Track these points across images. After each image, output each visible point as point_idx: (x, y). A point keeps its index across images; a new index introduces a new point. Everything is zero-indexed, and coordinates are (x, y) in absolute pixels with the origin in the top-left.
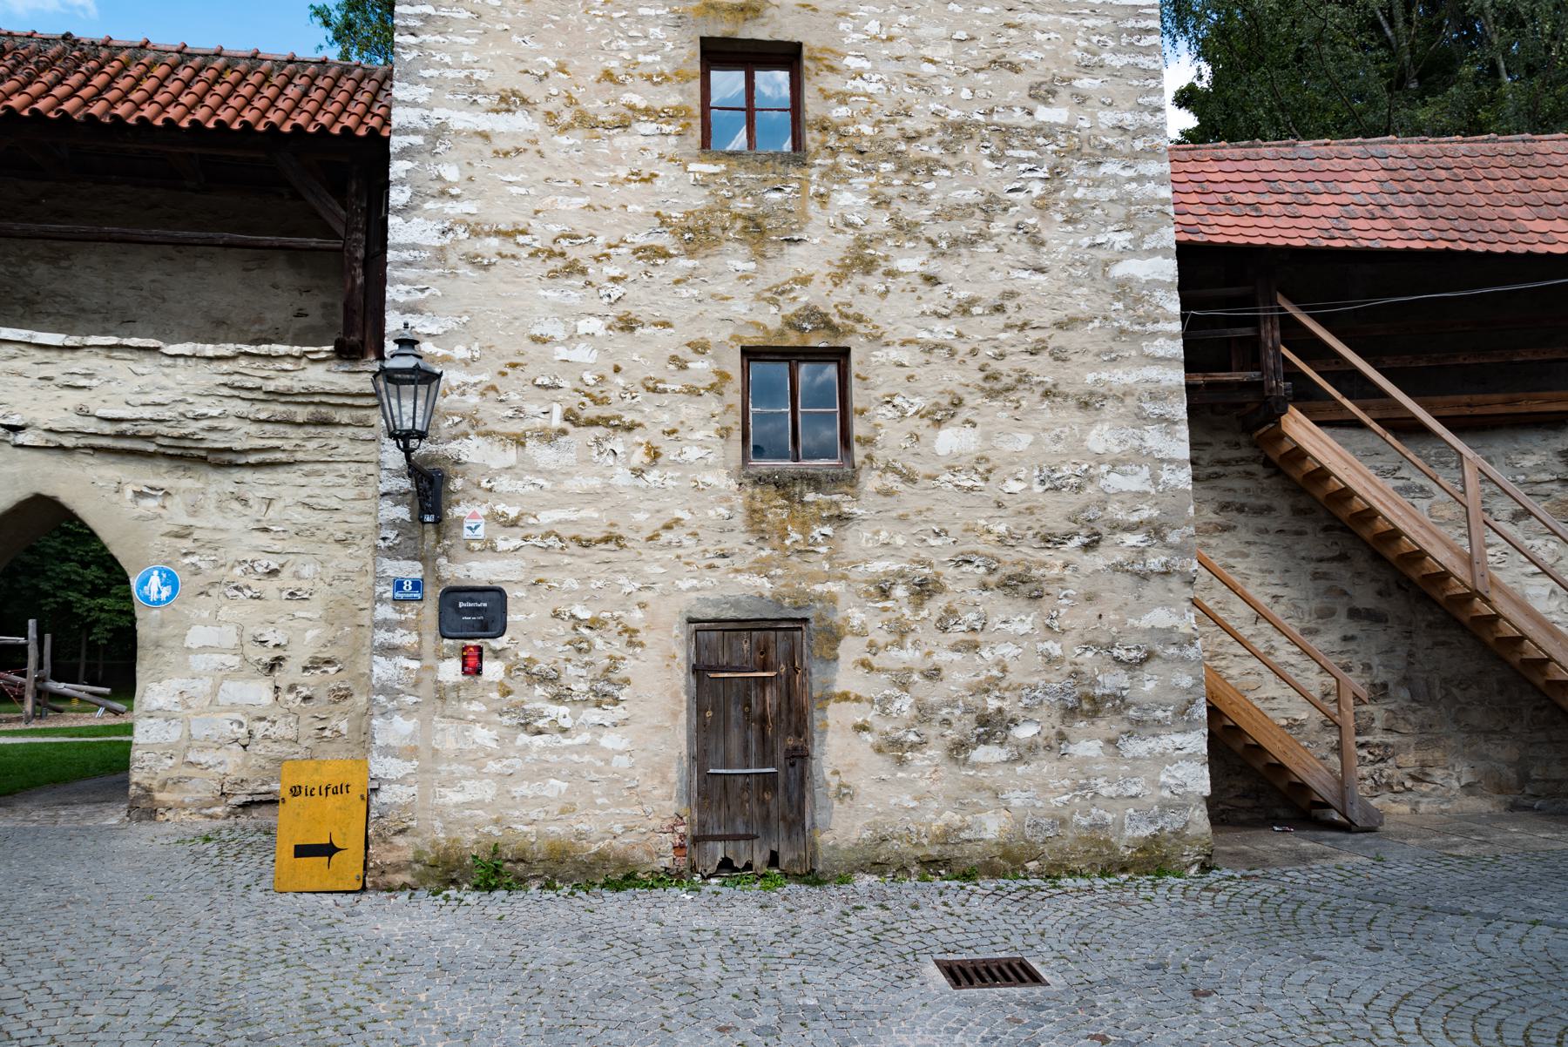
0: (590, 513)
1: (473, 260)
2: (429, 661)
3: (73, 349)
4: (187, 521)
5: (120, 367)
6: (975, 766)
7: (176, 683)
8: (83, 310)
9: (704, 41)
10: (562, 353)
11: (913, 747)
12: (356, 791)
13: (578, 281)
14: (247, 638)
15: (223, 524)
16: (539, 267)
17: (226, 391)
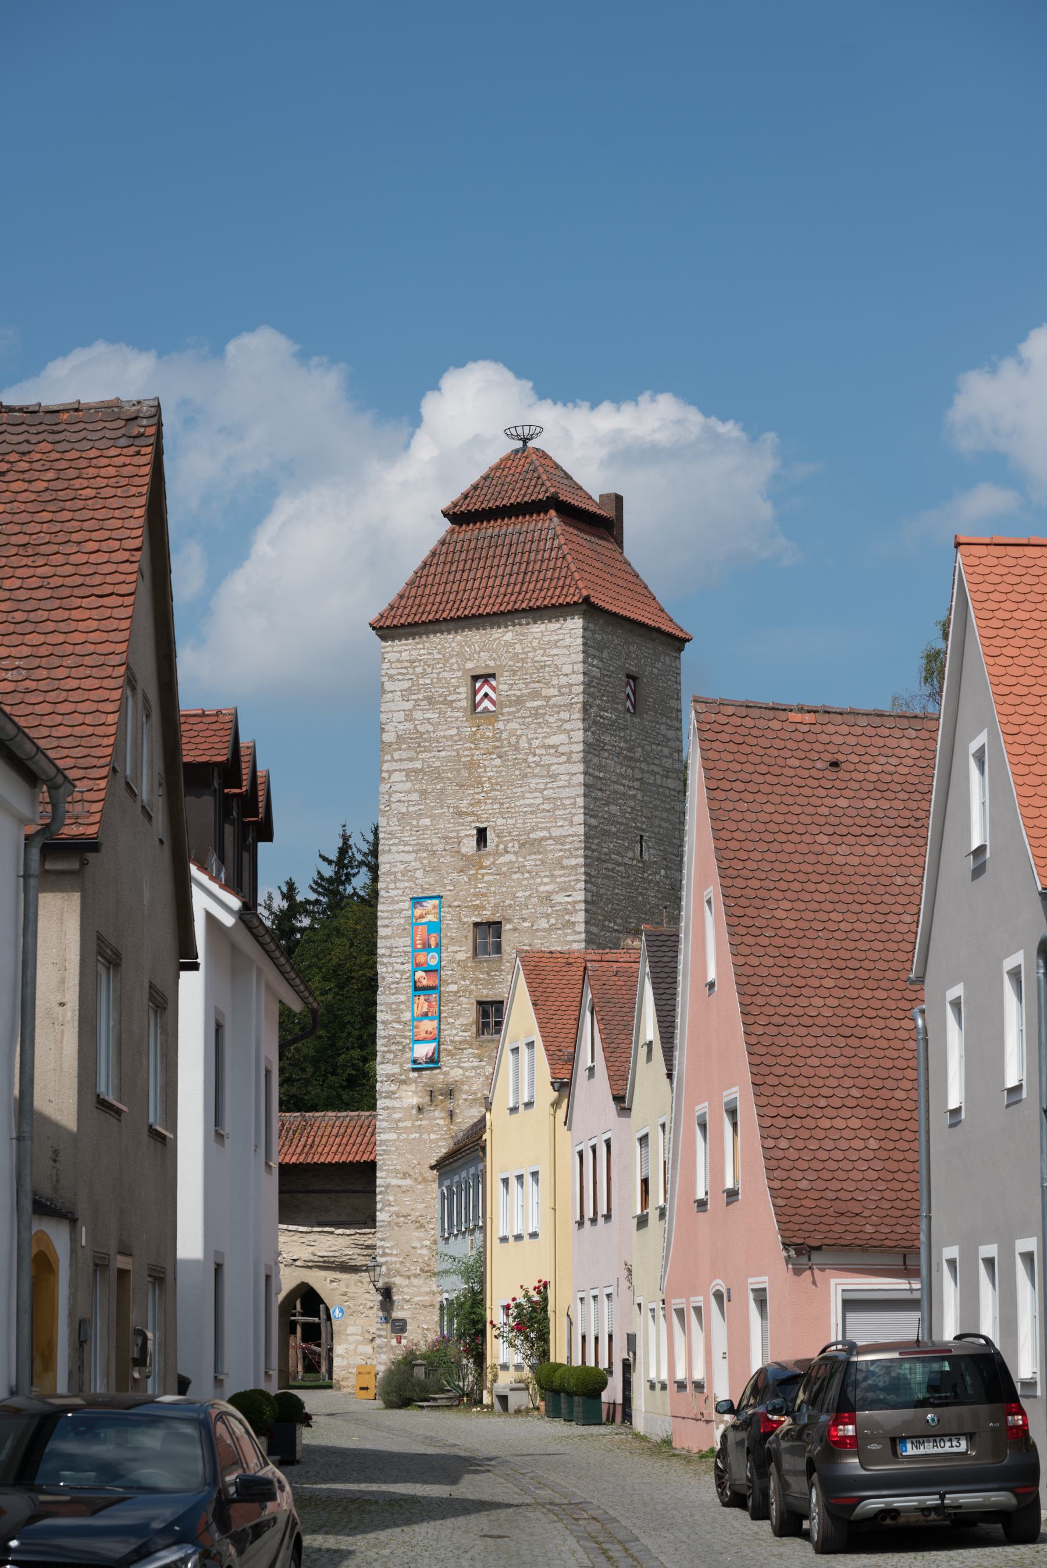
1: (397, 1224)
3: (309, 1233)
5: (323, 1238)
7: (345, 1346)
10: (419, 1251)
13: (423, 1230)
15: (356, 1291)
16: (413, 1226)
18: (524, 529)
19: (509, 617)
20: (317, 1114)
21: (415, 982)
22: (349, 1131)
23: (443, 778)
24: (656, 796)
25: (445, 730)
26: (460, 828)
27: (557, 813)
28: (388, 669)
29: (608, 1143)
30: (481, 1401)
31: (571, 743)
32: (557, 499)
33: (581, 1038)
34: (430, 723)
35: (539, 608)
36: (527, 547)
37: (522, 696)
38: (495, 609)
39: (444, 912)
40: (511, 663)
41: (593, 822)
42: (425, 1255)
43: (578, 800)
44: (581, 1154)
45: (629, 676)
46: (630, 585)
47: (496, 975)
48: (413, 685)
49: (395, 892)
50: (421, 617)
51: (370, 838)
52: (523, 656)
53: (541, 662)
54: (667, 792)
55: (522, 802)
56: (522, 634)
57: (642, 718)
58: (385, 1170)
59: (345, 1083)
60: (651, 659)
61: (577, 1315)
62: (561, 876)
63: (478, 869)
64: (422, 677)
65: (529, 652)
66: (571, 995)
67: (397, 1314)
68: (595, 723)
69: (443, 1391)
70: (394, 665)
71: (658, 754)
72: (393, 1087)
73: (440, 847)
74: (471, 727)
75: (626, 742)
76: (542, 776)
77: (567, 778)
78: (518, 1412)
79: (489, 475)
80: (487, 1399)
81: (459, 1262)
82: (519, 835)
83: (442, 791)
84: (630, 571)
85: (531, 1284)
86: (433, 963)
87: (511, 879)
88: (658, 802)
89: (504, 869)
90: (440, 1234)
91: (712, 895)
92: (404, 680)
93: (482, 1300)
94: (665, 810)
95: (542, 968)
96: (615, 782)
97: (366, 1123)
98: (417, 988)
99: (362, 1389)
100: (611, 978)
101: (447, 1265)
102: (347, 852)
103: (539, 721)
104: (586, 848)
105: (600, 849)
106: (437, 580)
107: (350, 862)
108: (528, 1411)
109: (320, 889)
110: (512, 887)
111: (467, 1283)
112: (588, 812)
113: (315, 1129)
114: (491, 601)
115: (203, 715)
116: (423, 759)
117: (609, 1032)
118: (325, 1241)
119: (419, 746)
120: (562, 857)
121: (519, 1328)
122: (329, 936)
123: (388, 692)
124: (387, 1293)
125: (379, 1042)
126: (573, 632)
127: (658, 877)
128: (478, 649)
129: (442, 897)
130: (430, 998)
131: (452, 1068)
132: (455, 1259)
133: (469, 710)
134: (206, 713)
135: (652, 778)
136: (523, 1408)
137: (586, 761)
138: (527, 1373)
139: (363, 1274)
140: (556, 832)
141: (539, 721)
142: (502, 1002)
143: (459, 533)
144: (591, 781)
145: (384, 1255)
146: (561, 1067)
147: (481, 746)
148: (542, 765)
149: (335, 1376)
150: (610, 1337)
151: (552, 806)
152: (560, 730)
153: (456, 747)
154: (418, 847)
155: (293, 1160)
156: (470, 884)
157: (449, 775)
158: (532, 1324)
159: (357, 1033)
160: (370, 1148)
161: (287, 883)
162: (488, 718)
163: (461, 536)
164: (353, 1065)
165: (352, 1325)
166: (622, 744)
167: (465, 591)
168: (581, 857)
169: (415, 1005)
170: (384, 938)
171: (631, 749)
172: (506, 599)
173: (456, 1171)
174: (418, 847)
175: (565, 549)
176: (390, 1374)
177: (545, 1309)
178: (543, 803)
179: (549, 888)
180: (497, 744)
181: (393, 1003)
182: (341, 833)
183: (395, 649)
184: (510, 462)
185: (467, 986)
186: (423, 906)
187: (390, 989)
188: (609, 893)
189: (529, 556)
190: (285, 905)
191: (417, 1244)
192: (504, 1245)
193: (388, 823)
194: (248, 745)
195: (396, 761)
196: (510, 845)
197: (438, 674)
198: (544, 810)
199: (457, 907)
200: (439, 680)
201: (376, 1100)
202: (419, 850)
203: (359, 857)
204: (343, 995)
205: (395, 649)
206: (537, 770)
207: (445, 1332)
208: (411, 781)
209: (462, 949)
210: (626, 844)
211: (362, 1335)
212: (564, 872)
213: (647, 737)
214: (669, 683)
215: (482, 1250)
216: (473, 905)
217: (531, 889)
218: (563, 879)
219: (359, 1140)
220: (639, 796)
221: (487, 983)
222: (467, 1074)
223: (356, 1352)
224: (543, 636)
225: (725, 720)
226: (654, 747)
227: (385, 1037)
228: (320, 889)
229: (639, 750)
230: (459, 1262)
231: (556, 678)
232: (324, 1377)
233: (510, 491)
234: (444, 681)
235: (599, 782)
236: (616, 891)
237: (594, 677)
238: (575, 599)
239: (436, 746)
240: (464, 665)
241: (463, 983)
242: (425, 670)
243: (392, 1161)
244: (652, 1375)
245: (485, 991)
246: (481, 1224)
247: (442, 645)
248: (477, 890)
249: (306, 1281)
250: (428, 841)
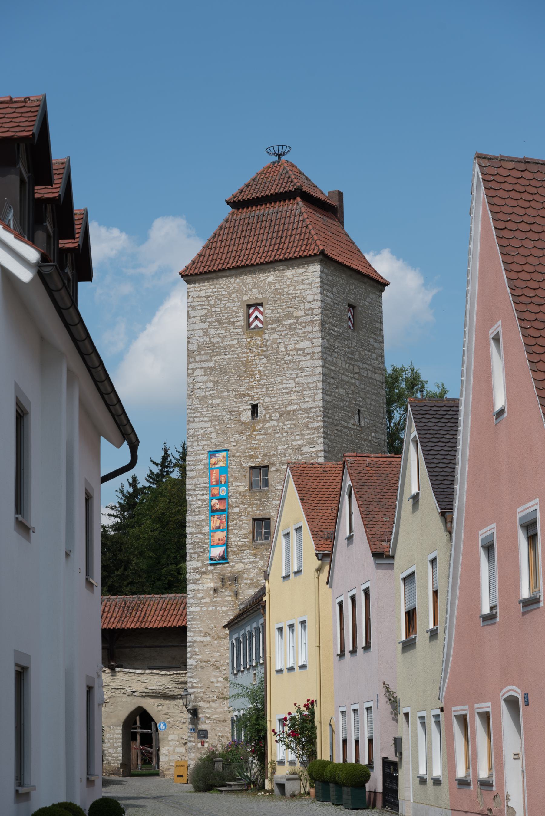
0: (221, 716)
1: (201, 667)
3: (143, 674)
4: (167, 711)
5: (152, 677)
7: (167, 748)
9: (454, 405)
10: (216, 685)
12: (186, 766)
13: (218, 670)
15: (174, 712)
16: (212, 668)
18: (280, 210)
19: (271, 265)
20: (148, 596)
21: (212, 507)
22: (169, 607)
23: (228, 372)
24: (368, 385)
25: (230, 341)
26: (240, 405)
27: (305, 393)
28: (191, 302)
29: (367, 592)
30: (263, 787)
31: (313, 347)
32: (302, 190)
33: (340, 517)
34: (219, 337)
35: (291, 258)
36: (282, 222)
37: (280, 317)
38: (262, 261)
39: (230, 460)
40: (273, 296)
41: (329, 399)
42: (220, 687)
43: (318, 384)
44: (341, 605)
45: (350, 306)
46: (349, 248)
47: (265, 501)
48: (208, 312)
49: (198, 448)
50: (213, 268)
51: (181, 450)
52: (281, 291)
53: (292, 294)
54: (375, 382)
55: (281, 386)
56: (280, 277)
57: (358, 333)
58: (193, 631)
59: (166, 586)
60: (364, 295)
61: (338, 724)
62: (308, 434)
63: (253, 431)
64: (214, 307)
65: (285, 288)
66: (328, 493)
67: (202, 727)
68: (329, 334)
69: (235, 779)
70: (195, 300)
71: (369, 357)
72: (198, 577)
73: (227, 418)
74: (247, 338)
75: (349, 348)
76: (294, 369)
77: (311, 369)
78: (293, 796)
79: (256, 177)
80: (268, 786)
81: (247, 689)
82: (280, 408)
83: (228, 381)
84: (349, 240)
85: (302, 702)
86: (223, 493)
87: (275, 438)
88: (370, 389)
89: (270, 431)
90: (231, 671)
91: (500, 330)
92: (202, 309)
93: (264, 715)
94: (374, 394)
95: (306, 475)
96: (342, 374)
97: (180, 601)
98: (213, 511)
99: (178, 776)
100: (365, 469)
101: (236, 691)
102: (167, 459)
104: (324, 416)
105: (333, 417)
106: (223, 244)
107: (169, 464)
108: (301, 795)
109: (151, 480)
110: (275, 442)
111: (252, 703)
112: (325, 392)
113: (146, 606)
114: (259, 256)
115: (11, 101)
116: (215, 361)
117: (366, 506)
118: (153, 679)
119: (213, 352)
120: (308, 422)
121: (293, 734)
122: (156, 497)
123: (192, 317)
124: (194, 712)
125: (188, 547)
126: (313, 274)
127: (370, 438)
128: (251, 287)
129: (228, 450)
130: (222, 517)
131: (237, 563)
132: (244, 687)
133: (245, 327)
134: (14, 100)
135: (366, 372)
136: (296, 793)
137: (323, 359)
138: (298, 767)
139: (179, 700)
140: (304, 406)
142: (269, 519)
143: (237, 214)
144: (327, 372)
145: (193, 687)
146: (323, 543)
147: (254, 350)
148: (294, 362)
149: (161, 768)
150: (370, 741)
151: (301, 388)
152: (306, 339)
153: (236, 352)
154: (213, 418)
155: (132, 626)
156: (248, 441)
157: (233, 370)
158: (303, 732)
159: (173, 555)
160: (182, 618)
161: (132, 477)
162: (258, 332)
163: (239, 216)
164: (172, 575)
166: (347, 349)
167: (242, 250)
168: (321, 421)
169: (212, 522)
170: (191, 478)
171: (352, 353)
172: (269, 254)
173: (242, 627)
174: (213, 418)
175: (308, 221)
176: (198, 768)
177: (312, 721)
178: (295, 387)
179: (300, 442)
180: (264, 349)
181: (197, 521)
182: (163, 447)
183: (196, 289)
184: (270, 169)
185: (246, 509)
186: (216, 457)
187: (195, 511)
188: (339, 446)
189: (283, 227)
190: (131, 490)
191: (214, 680)
192: (280, 675)
193: (193, 403)
194: (63, 161)
195: (197, 362)
196: (273, 415)
197: (225, 304)
198: (296, 391)
199: (238, 457)
200: (226, 308)
201: (186, 585)
202: (213, 420)
203: (174, 461)
204: (164, 532)
205: (196, 289)
206: (291, 365)
207: (235, 738)
208: (208, 375)
209: (242, 484)
210: (350, 415)
211: (178, 740)
212: (310, 432)
213: (362, 346)
214: (375, 312)
215: (263, 679)
217: (288, 444)
218: (309, 436)
219: (175, 612)
220: (358, 383)
221: (259, 506)
222: (246, 567)
224: (294, 277)
225: (507, 173)
226: (366, 352)
227: (192, 544)
228: (151, 480)
229: (357, 353)
230: (247, 689)
231: (303, 304)
232: (155, 767)
233: (270, 187)
234: (228, 309)
235: (332, 373)
236: (344, 445)
237: (328, 304)
238: (315, 252)
239: (224, 352)
240: (242, 298)
241: (243, 506)
242: (216, 302)
243: (197, 625)
244: (422, 771)
245: (258, 512)
246: (262, 661)
247: (227, 286)
248: (252, 445)
249: (141, 706)
250: (219, 414)
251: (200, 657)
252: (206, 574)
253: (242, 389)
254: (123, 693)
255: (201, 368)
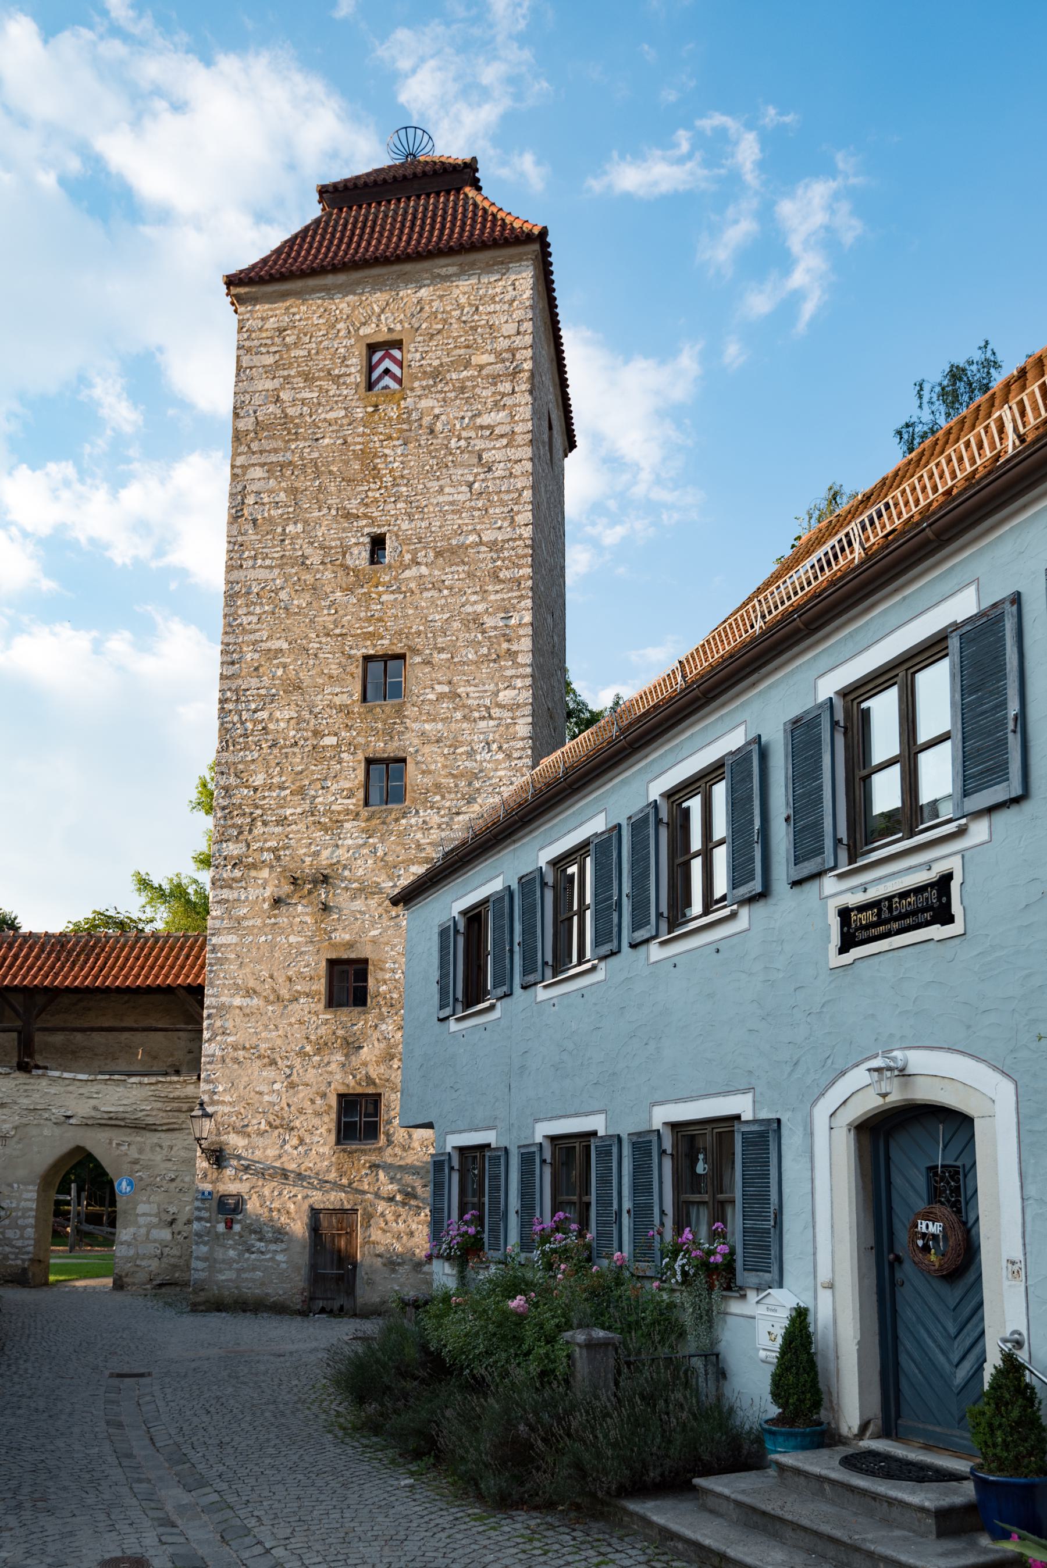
1: (236, 1060)
2: (214, 1223)
4: (137, 1156)
5: (111, 1088)
6: (424, 1273)
7: (132, 1230)
8: (96, 1055)
11: (399, 1264)
13: (273, 1067)
14: (161, 1210)
17: (153, 1098)
48: (281, 358)
70: (254, 335)
103: (466, 395)
133: (363, 385)
141: (466, 395)
142: (404, 760)
165: (145, 1203)
179: (480, 608)
180: (405, 426)
191: (264, 1088)
211: (157, 1215)
212: (502, 586)
216: (363, 633)
221: (389, 734)
223: (147, 1238)
242: (298, 338)
249: (82, 1144)
251: (230, 1039)
252: (256, 869)
253: (353, 506)
254: (46, 1119)
255: (262, 465)
